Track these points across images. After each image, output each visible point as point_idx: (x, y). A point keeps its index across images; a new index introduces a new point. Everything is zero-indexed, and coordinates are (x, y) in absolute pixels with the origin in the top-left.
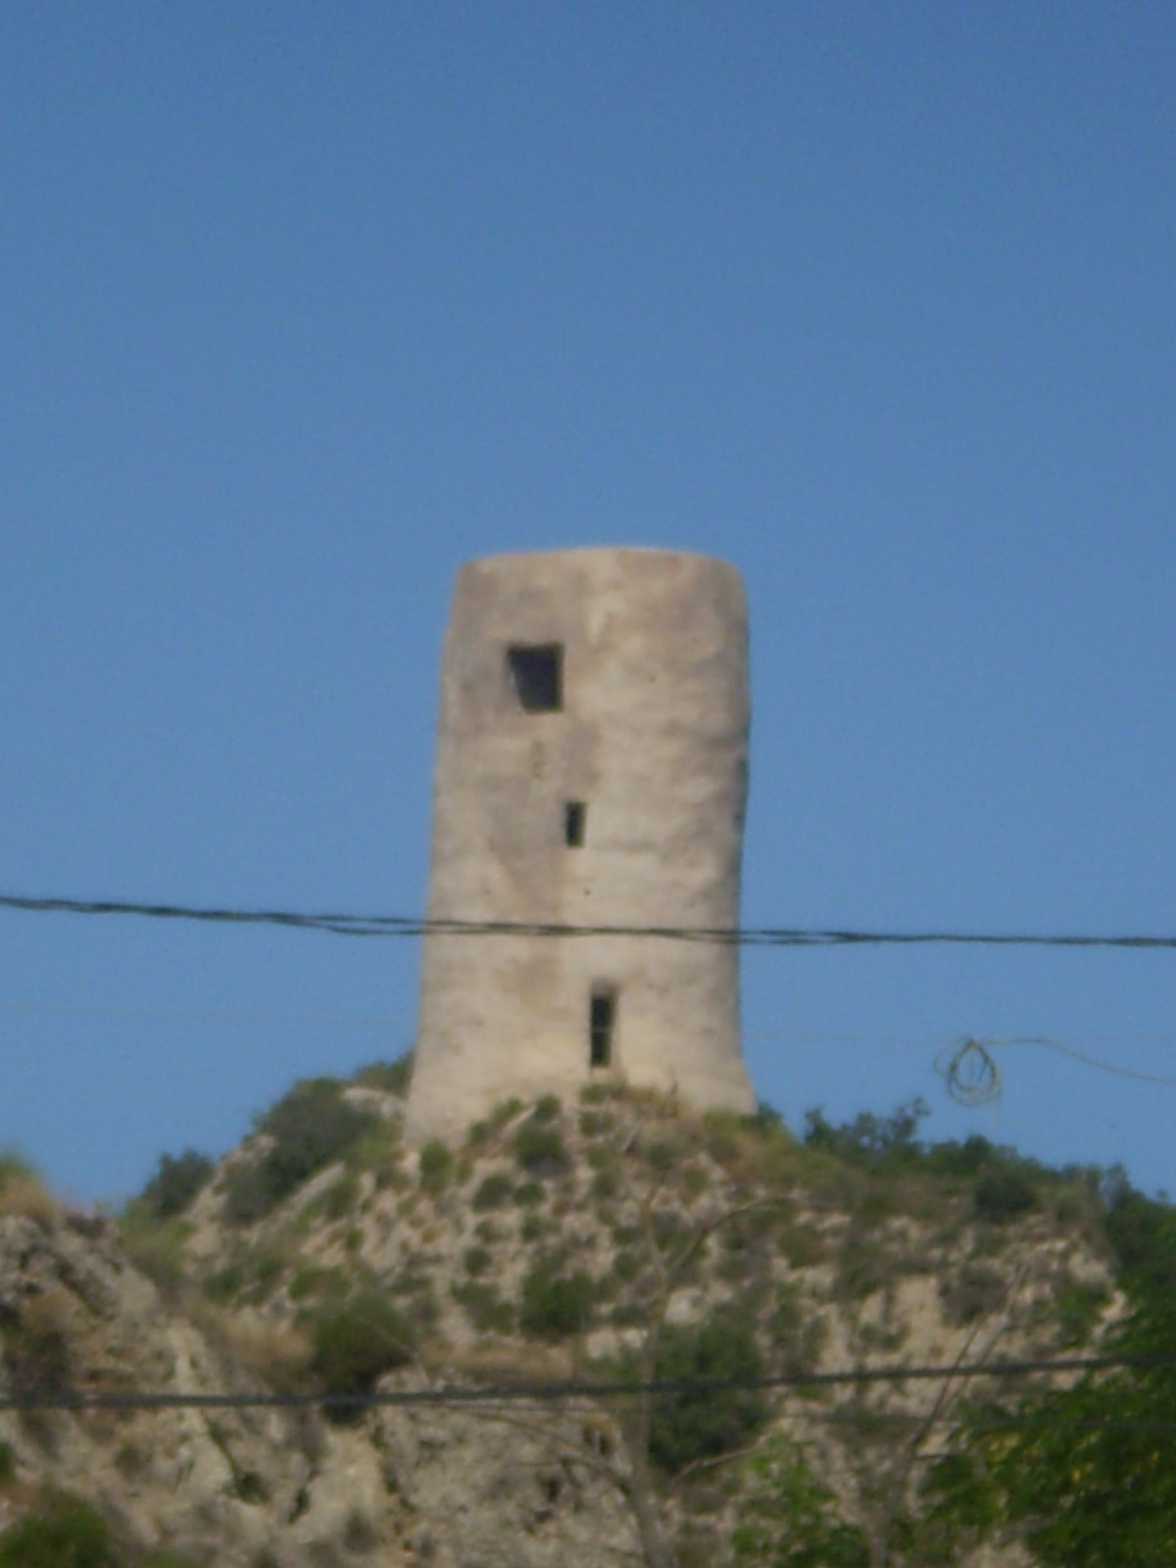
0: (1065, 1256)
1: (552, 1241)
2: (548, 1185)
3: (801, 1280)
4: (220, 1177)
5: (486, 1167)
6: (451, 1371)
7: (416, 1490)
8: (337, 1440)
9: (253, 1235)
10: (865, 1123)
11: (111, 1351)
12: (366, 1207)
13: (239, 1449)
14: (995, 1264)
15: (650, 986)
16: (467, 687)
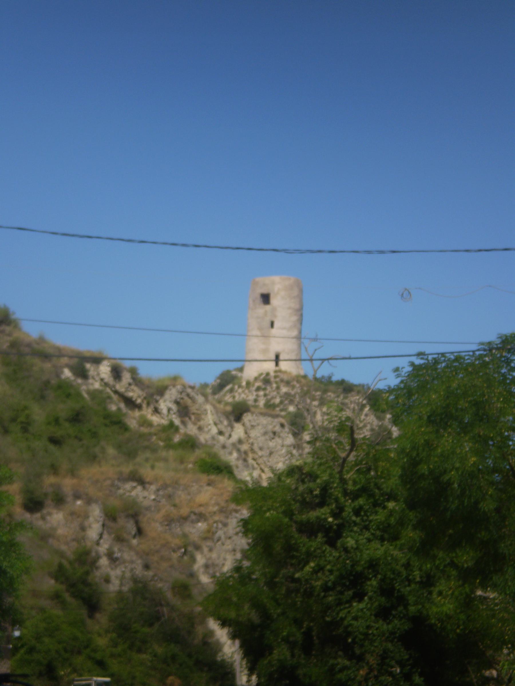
0: (359, 399)
1: (269, 397)
4: (210, 387)
5: (257, 384)
7: (251, 434)
9: (216, 397)
10: (323, 377)
11: (197, 410)
12: (236, 391)
14: (346, 401)
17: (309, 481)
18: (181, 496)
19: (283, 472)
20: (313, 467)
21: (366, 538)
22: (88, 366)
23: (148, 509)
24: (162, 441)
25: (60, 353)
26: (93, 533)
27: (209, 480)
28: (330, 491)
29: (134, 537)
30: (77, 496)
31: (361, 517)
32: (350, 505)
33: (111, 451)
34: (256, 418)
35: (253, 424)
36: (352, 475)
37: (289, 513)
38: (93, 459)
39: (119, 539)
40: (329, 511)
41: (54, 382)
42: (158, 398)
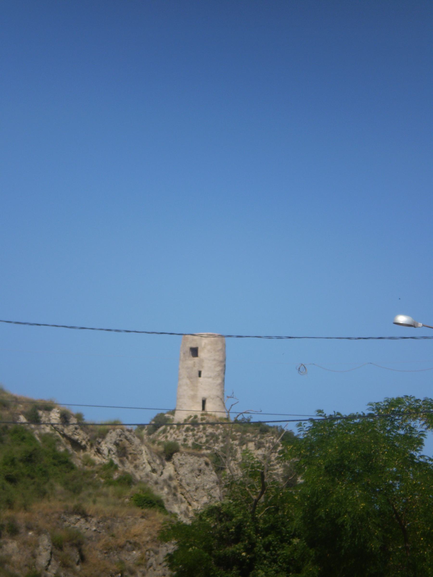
0: (273, 439)
1: (196, 437)
2: (196, 428)
3: (234, 443)
6: (185, 453)
7: (179, 471)
8: (167, 463)
9: (151, 437)
11: (133, 450)
12: (168, 432)
13: (152, 465)
14: (263, 440)
15: (211, 398)
16: (184, 354)
17: (226, 520)
18: (119, 527)
19: (204, 512)
20: (229, 508)
21: (274, 570)
22: (40, 413)
23: (89, 539)
24: (103, 478)
25: (17, 401)
26: (42, 560)
27: (143, 513)
28: (243, 529)
29: (78, 564)
30: (29, 528)
31: (270, 552)
32: (261, 541)
33: (59, 488)
34: (184, 457)
35: (182, 462)
36: (263, 515)
37: (208, 549)
38: (43, 494)
39: (65, 565)
40: (242, 546)
41: (11, 427)
42: (100, 440)
